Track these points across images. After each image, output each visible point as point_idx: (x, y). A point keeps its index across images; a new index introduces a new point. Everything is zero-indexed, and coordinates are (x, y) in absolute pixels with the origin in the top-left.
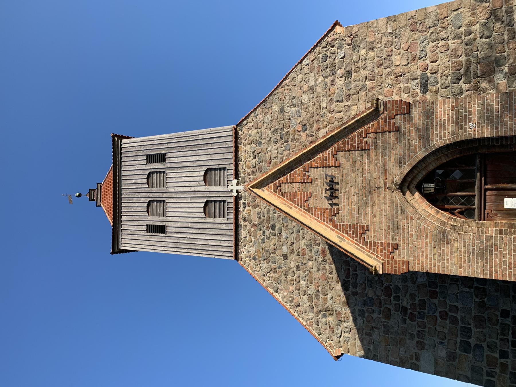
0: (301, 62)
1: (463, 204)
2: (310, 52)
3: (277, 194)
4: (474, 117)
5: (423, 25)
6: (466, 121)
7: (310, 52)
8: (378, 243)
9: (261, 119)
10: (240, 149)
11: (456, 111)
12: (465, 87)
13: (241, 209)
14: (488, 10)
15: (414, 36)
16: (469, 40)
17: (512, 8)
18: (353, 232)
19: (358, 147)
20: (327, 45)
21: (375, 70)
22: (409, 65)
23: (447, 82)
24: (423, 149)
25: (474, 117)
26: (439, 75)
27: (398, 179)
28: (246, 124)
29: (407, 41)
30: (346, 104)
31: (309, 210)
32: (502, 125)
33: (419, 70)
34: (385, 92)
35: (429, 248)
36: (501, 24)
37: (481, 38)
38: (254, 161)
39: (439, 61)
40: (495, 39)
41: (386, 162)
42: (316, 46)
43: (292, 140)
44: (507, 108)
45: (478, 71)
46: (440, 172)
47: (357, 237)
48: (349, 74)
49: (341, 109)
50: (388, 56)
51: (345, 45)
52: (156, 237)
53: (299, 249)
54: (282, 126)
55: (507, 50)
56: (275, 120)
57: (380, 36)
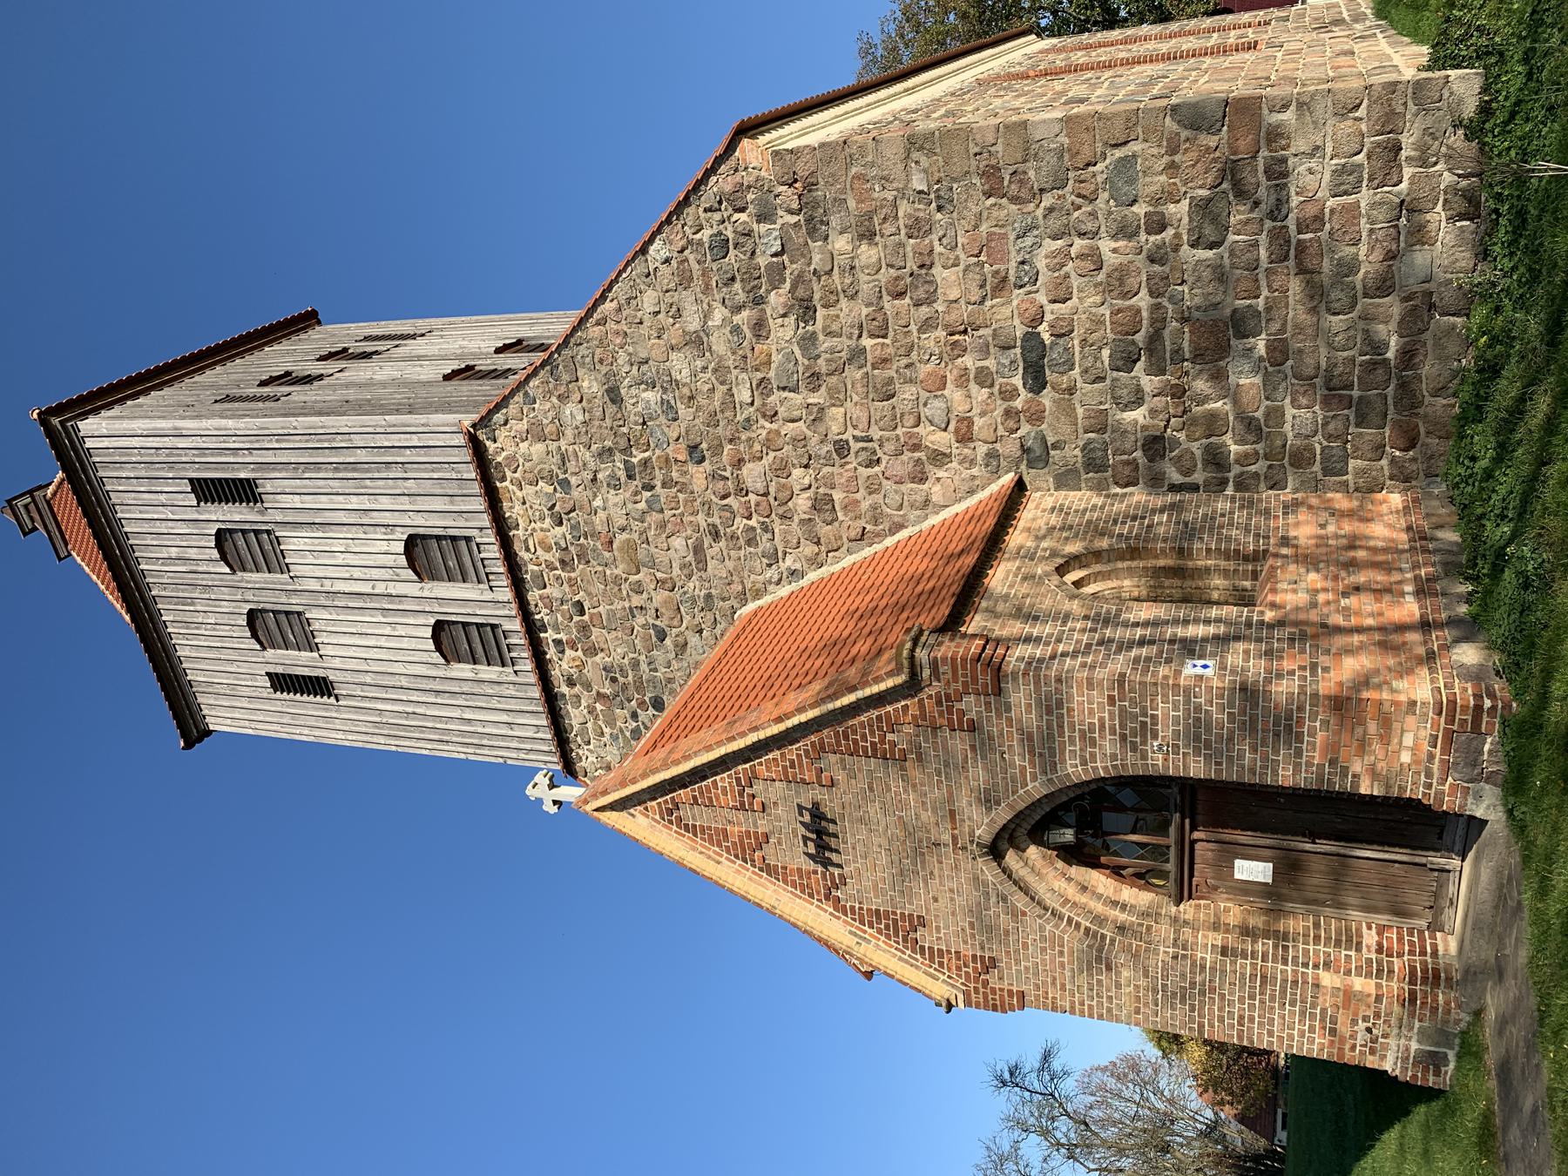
0: (643, 251)
1: (1141, 857)
2: (668, 221)
4: (1165, 732)
5: (1021, 181)
6: (1144, 736)
7: (668, 221)
8: (949, 952)
9: (551, 414)
10: (504, 496)
11: (1121, 711)
12: (1149, 383)
13: (551, 653)
14: (1215, 160)
15: (995, 214)
16: (1159, 247)
17: (1284, 160)
20: (720, 202)
21: (887, 306)
22: (988, 303)
23: (1098, 364)
24: (1041, 778)
25: (1165, 732)
26: (1076, 342)
28: (506, 423)
29: (976, 227)
30: (810, 401)
32: (1230, 759)
33: (1017, 322)
34: (921, 377)
35: (1068, 974)
36: (1252, 210)
37: (1192, 246)
38: (559, 530)
39: (1075, 299)
40: (1232, 253)
41: (951, 794)
42: (686, 202)
43: (664, 485)
44: (1244, 723)
45: (1186, 345)
48: (806, 310)
49: (796, 414)
50: (922, 266)
51: (780, 213)
52: (308, 705)
54: (623, 443)
55: (1265, 292)
56: (597, 423)
57: (890, 195)
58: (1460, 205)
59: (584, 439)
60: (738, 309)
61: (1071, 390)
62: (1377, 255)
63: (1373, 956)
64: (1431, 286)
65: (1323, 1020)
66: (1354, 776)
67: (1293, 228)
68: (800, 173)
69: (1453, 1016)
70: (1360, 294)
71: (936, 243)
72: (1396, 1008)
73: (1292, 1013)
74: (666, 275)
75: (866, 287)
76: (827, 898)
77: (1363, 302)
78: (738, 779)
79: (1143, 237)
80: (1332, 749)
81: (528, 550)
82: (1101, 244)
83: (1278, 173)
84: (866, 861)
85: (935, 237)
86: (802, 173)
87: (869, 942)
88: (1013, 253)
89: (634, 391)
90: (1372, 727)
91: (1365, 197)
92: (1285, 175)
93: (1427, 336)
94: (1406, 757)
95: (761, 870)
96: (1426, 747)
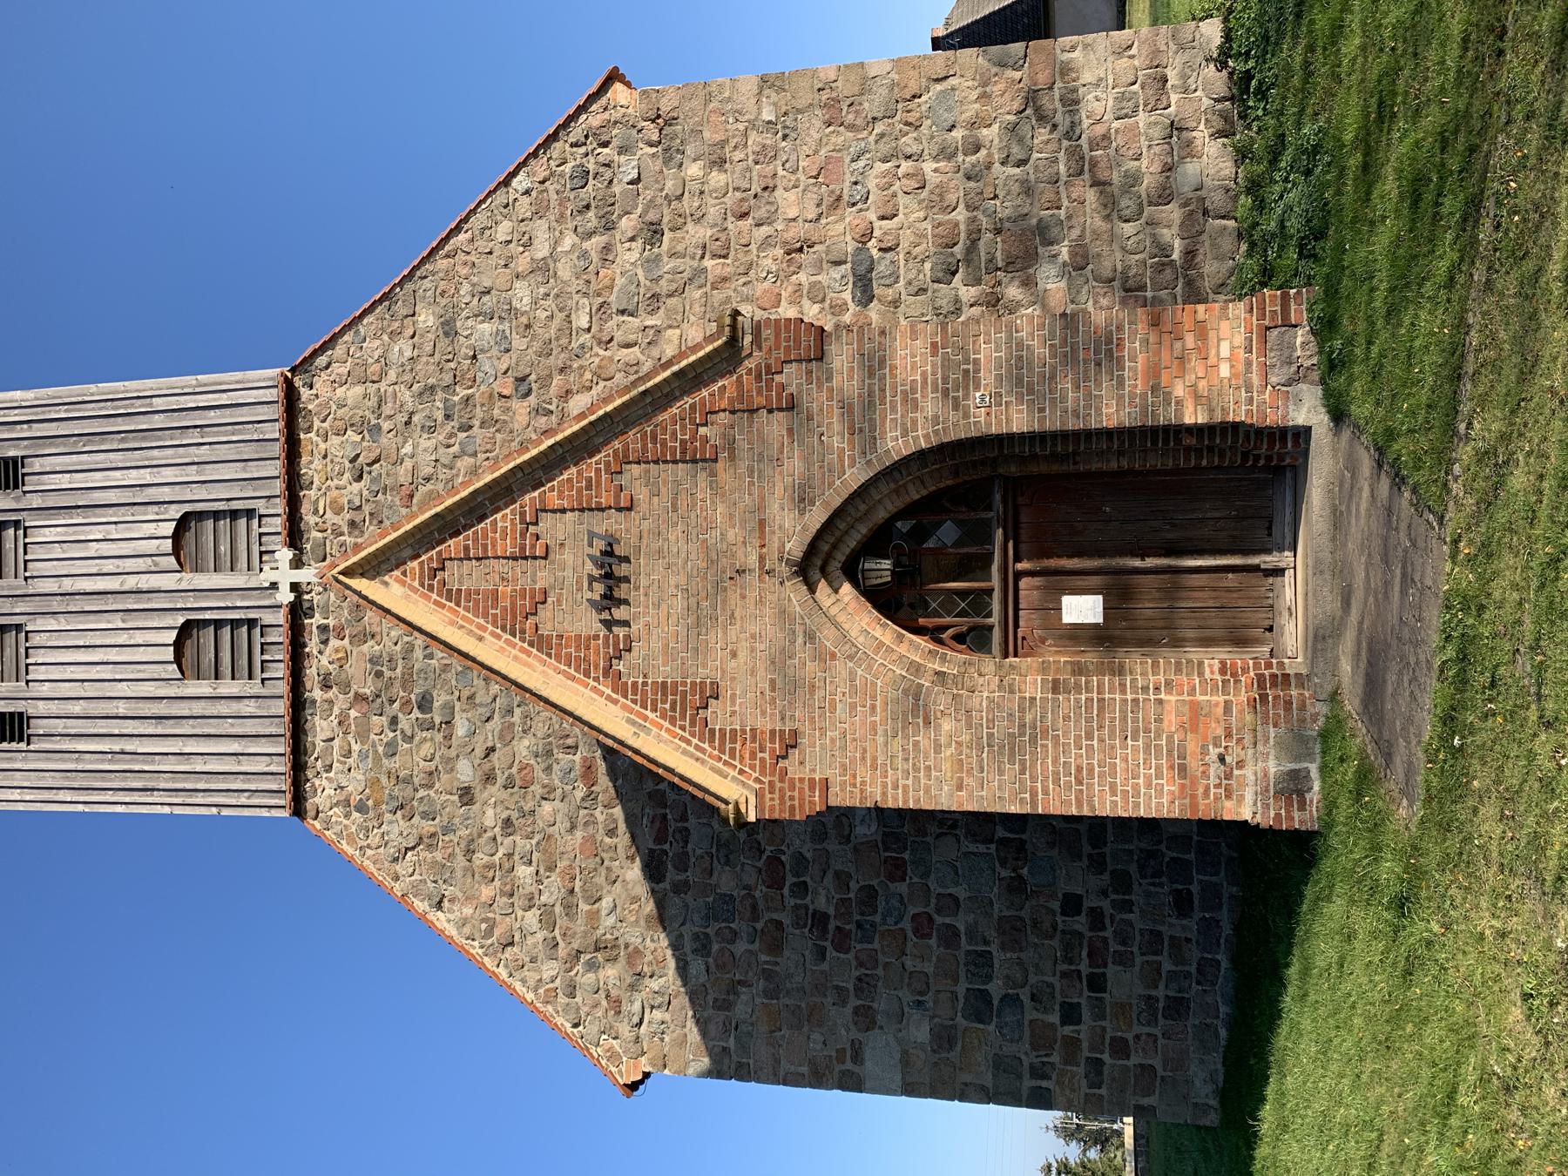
0: (506, 183)
2: (535, 154)
3: (434, 596)
5: (857, 112)
6: (966, 388)
7: (535, 154)
8: (744, 732)
10: (305, 449)
13: (312, 646)
14: (1020, 90)
17: (1075, 90)
18: (674, 703)
19: (684, 452)
20: (587, 137)
21: (730, 226)
22: (823, 221)
27: (795, 547)
28: (327, 367)
29: (816, 152)
30: (648, 323)
31: (541, 643)
32: (1053, 401)
33: (848, 238)
35: (880, 740)
36: (1051, 132)
38: (356, 486)
41: (762, 498)
42: (554, 137)
43: (483, 424)
45: (998, 254)
46: (903, 526)
47: (683, 717)
48: (654, 232)
49: (632, 337)
51: (641, 145)
53: (511, 767)
56: (424, 359)
57: (741, 127)
58: (1218, 124)
59: (407, 377)
60: (590, 235)
61: (896, 303)
62: (1156, 167)
63: (1218, 677)
64: (1203, 193)
65: (1170, 752)
66: (1177, 403)
67: (1086, 147)
68: (663, 109)
69: (1310, 710)
70: (1145, 203)
71: (780, 168)
72: (1248, 718)
73: (1135, 749)
74: (524, 207)
75: (713, 212)
76: (606, 674)
77: (1148, 210)
78: (523, 514)
79: (960, 158)
80: (1154, 371)
81: (316, 512)
82: (924, 165)
83: (1071, 102)
84: (656, 614)
85: (779, 163)
86: (664, 109)
87: (648, 732)
88: (848, 175)
89: (470, 323)
90: (1190, 341)
91: (1142, 118)
92: (1077, 102)
93: (1204, 237)
94: (1225, 370)
95: (531, 644)
96: (1242, 355)
